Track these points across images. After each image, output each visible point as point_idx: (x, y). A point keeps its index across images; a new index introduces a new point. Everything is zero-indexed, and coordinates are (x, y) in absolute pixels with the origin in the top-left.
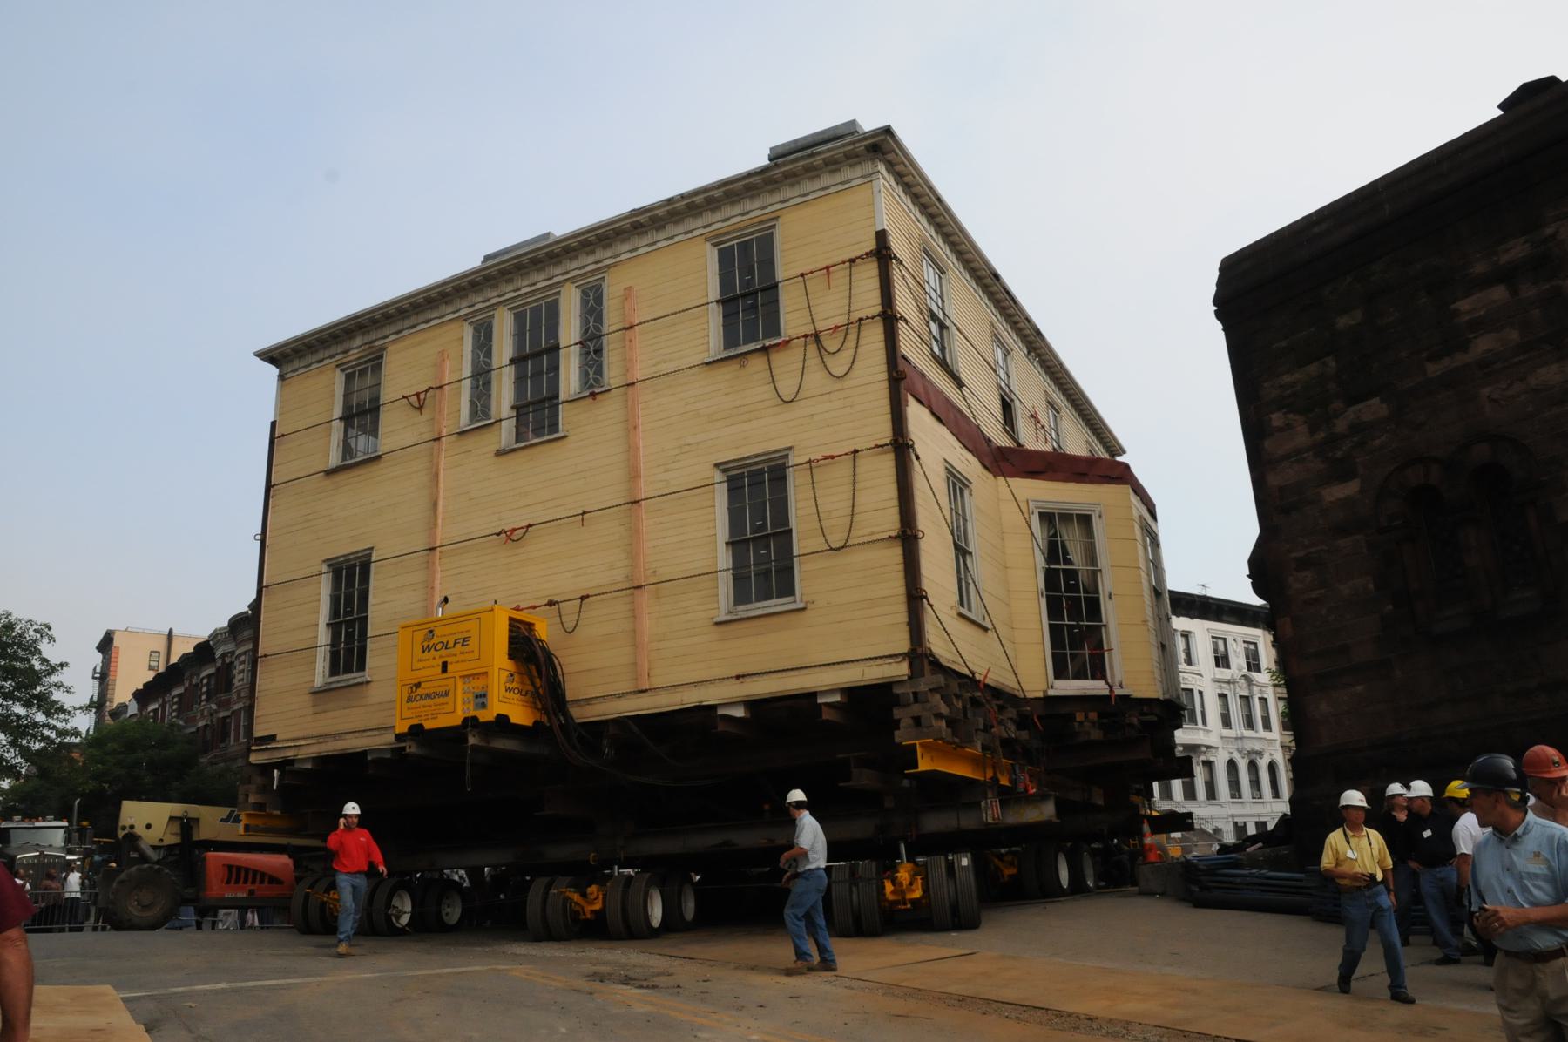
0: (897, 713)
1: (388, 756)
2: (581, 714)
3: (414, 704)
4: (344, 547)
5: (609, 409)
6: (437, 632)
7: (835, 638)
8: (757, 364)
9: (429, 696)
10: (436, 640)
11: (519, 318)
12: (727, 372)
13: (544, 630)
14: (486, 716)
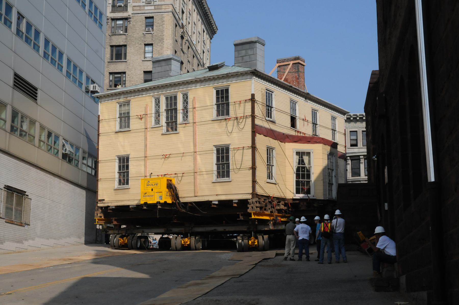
0: (248, 206)
2: (182, 200)
4: (122, 153)
5: (190, 128)
6: (150, 182)
7: (237, 188)
8: (224, 123)
9: (148, 196)
11: (167, 98)
12: (216, 125)
13: (174, 182)
14: (162, 201)
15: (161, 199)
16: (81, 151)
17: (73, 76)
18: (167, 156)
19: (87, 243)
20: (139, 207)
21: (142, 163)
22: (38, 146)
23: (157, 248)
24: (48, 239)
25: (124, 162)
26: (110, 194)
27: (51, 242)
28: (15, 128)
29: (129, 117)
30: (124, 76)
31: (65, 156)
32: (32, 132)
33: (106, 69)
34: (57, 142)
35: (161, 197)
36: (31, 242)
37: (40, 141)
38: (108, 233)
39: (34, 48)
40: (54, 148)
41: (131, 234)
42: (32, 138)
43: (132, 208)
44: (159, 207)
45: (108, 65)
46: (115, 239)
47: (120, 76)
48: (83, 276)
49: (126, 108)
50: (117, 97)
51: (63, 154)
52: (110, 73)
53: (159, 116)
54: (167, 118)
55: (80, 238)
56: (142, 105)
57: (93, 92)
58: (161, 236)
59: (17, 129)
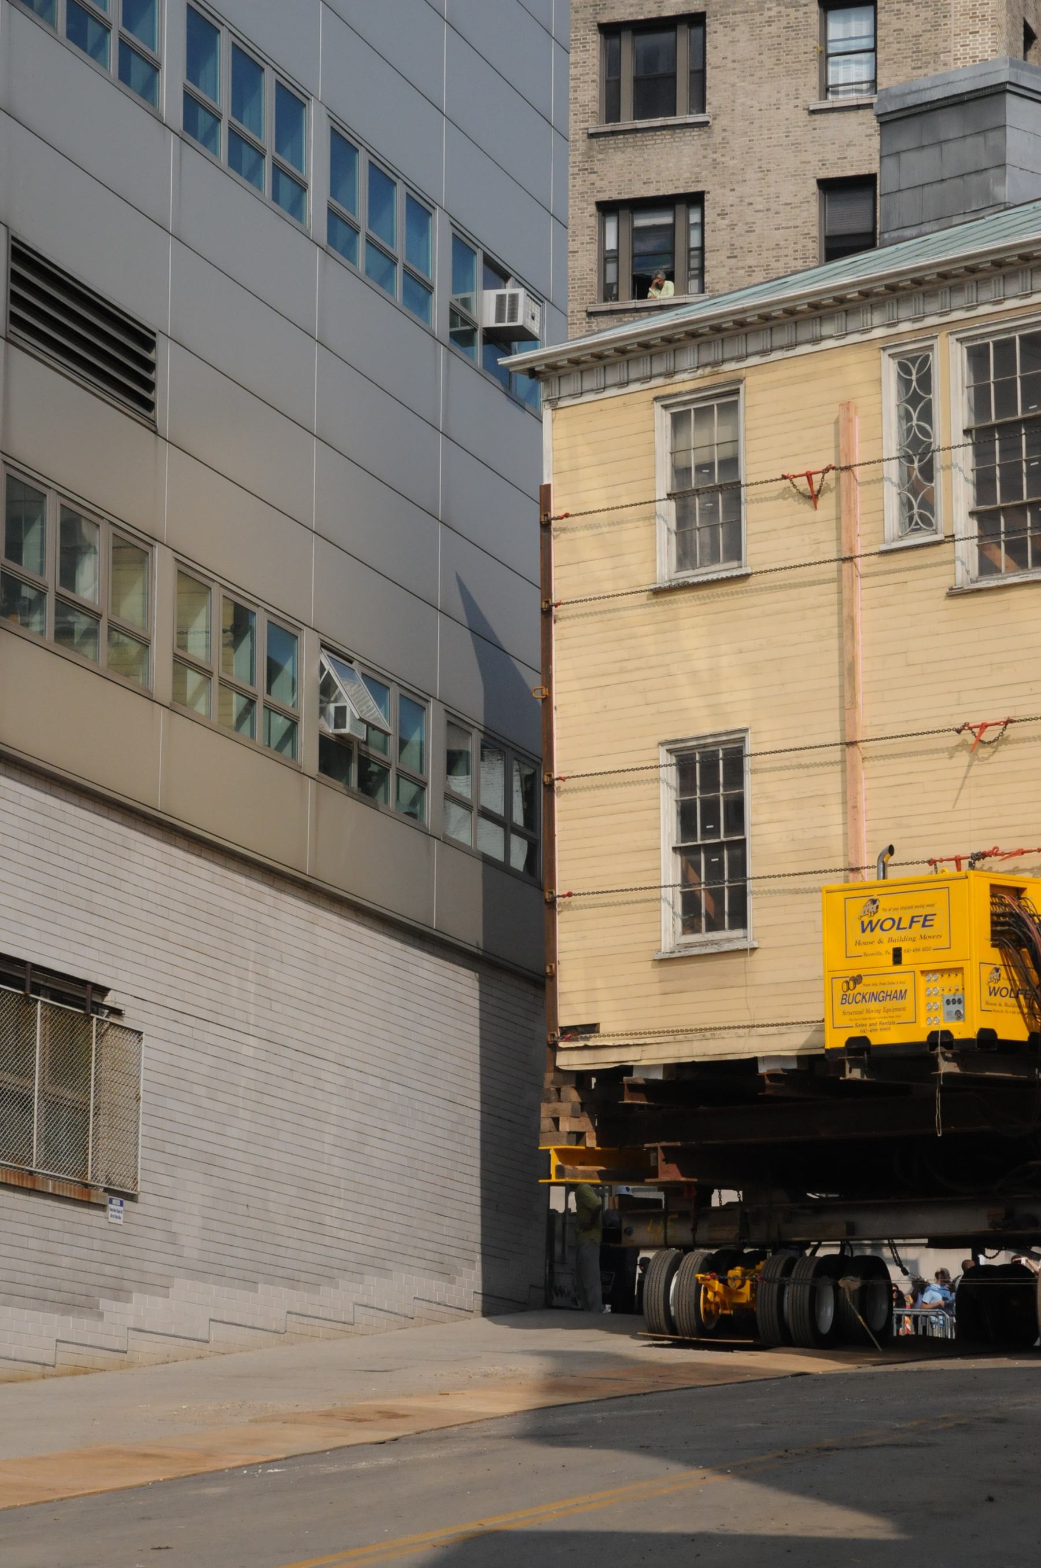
1: (794, 1066)
3: (854, 1007)
4: (701, 724)
6: (883, 902)
9: (875, 997)
10: (881, 915)
11: (977, 356)
14: (964, 1030)
15: (959, 1016)
16: (433, 715)
17: (370, 241)
18: (988, 735)
19: (498, 1304)
20: (815, 1072)
21: (831, 782)
22: (167, 698)
23: (944, 1341)
24: (252, 1285)
25: (711, 782)
26: (628, 991)
27: (272, 1303)
28: (27, 592)
29: (733, 491)
30: (695, 217)
31: (335, 755)
32: (130, 611)
33: (577, 184)
34: (288, 667)
35: (955, 1003)
36: (143, 1308)
37: (182, 663)
38: (626, 1241)
39: (124, 75)
40: (270, 709)
41: (779, 1245)
42: (133, 648)
43: (772, 1076)
44: (946, 1067)
45: (588, 157)
46: (676, 1279)
47: (665, 219)
48: (472, 1526)
49: (717, 430)
50: (659, 367)
51: (324, 741)
52: (607, 208)
53: (928, 472)
54: (983, 483)
55: (446, 1273)
56: (819, 410)
57: (503, 339)
58: (967, 1254)
59: (42, 595)
